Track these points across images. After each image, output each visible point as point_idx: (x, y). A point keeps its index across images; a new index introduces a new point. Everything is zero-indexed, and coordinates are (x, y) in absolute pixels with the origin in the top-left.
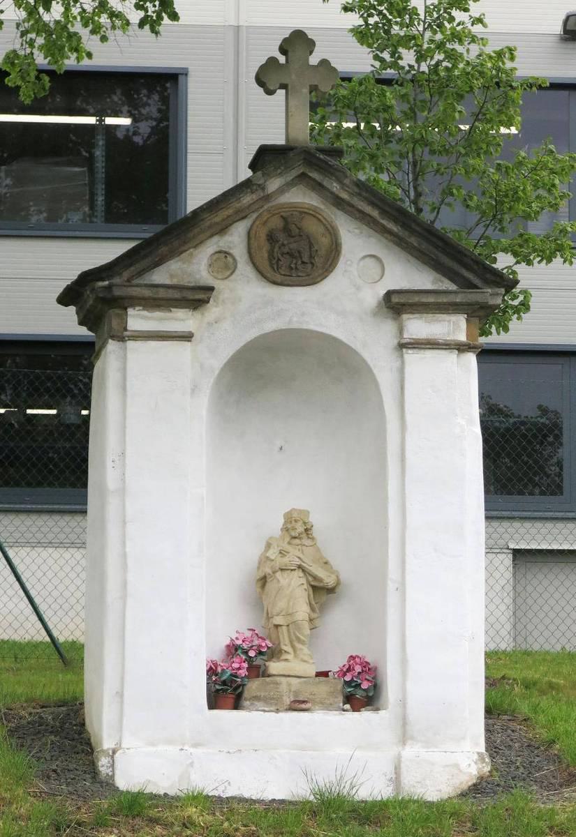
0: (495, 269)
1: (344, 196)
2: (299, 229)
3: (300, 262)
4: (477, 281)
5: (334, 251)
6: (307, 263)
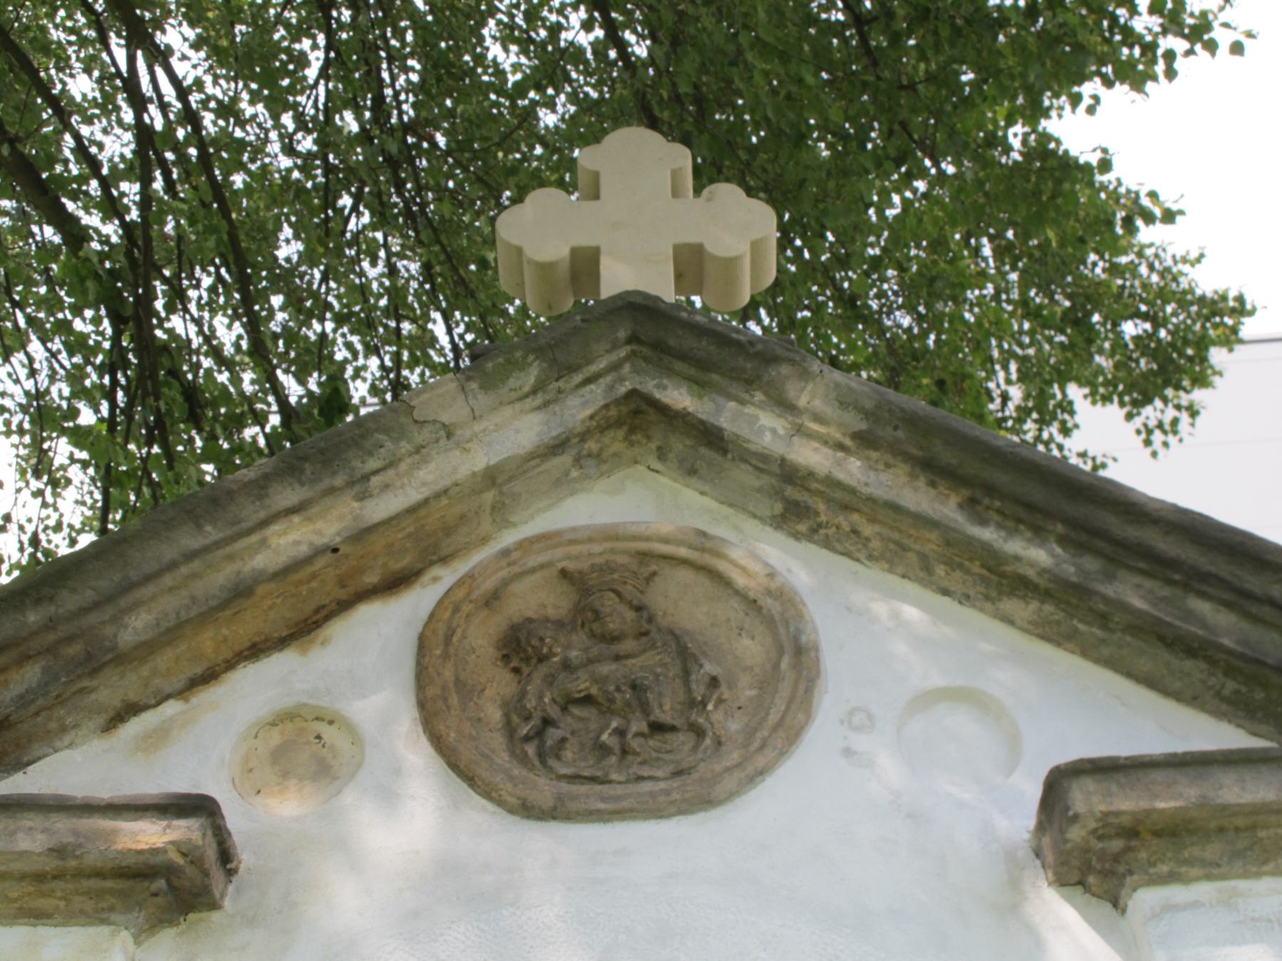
0: (215, 379)
1: (811, 456)
2: (639, 609)
3: (638, 725)
6: (673, 729)
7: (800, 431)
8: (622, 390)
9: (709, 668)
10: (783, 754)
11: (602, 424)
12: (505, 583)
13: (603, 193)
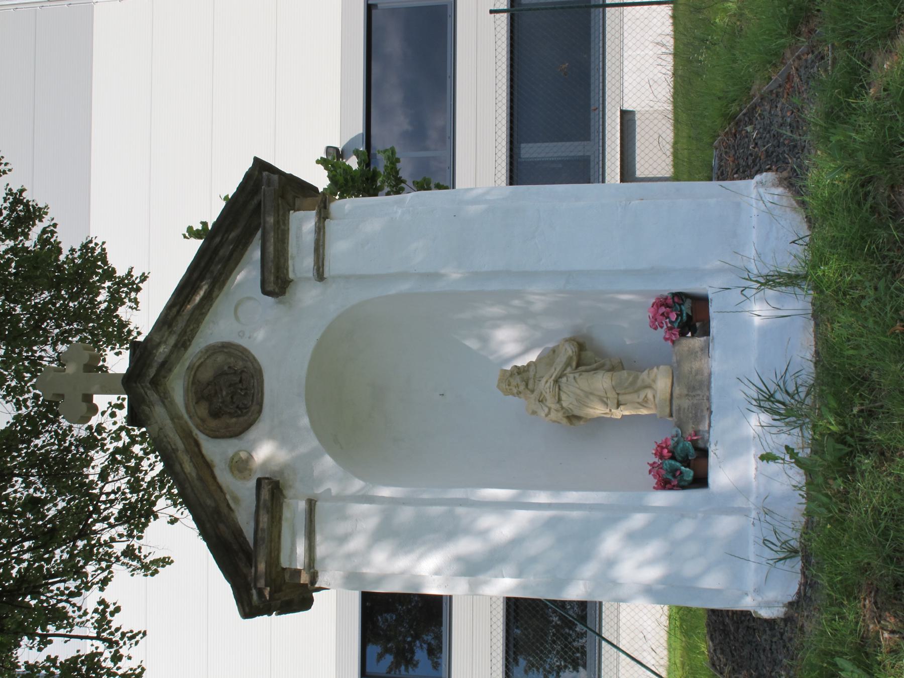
1: (172, 340)
3: (240, 386)
4: (255, 202)
5: (226, 348)
6: (241, 378)
7: (165, 342)
8: (149, 386)
9: (226, 368)
10: (249, 352)
11: (157, 392)
12: (198, 417)
13: (61, 392)
